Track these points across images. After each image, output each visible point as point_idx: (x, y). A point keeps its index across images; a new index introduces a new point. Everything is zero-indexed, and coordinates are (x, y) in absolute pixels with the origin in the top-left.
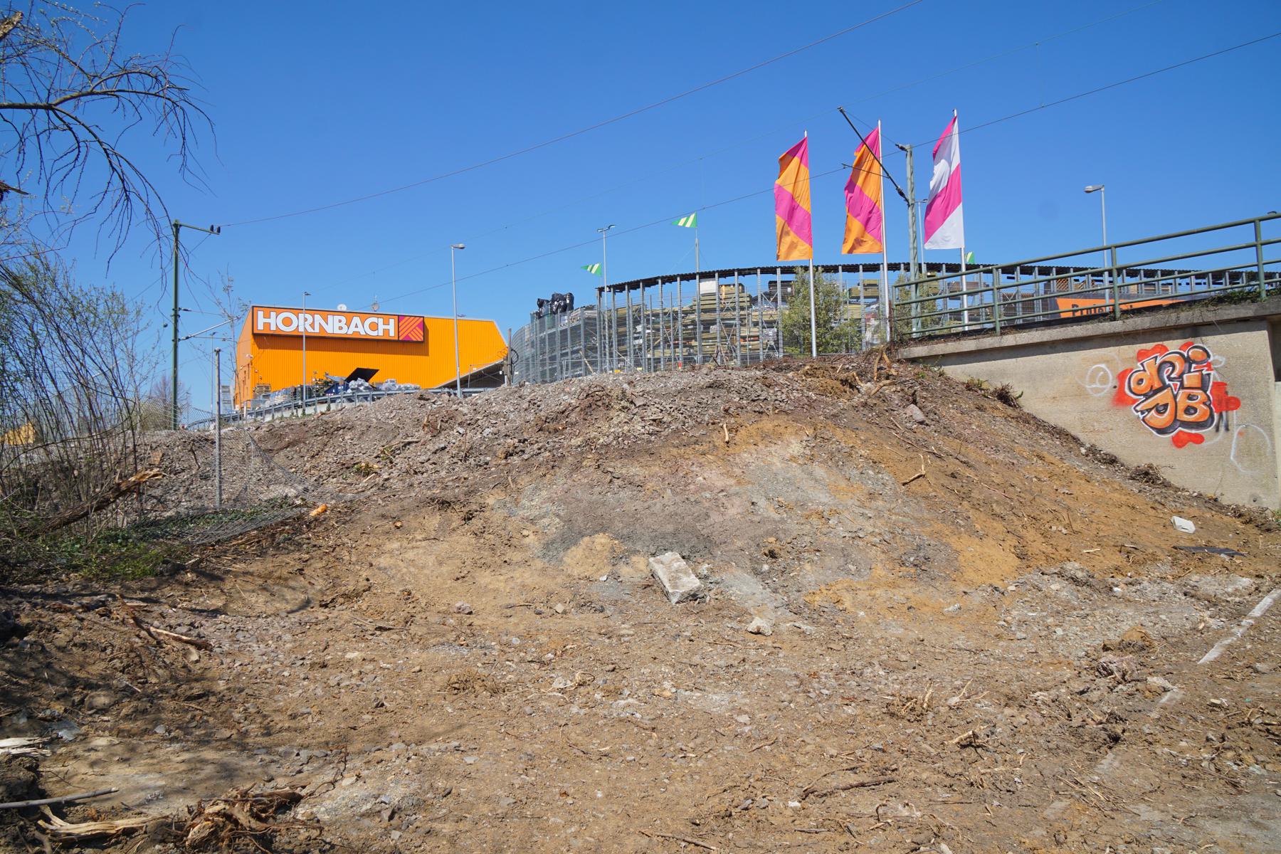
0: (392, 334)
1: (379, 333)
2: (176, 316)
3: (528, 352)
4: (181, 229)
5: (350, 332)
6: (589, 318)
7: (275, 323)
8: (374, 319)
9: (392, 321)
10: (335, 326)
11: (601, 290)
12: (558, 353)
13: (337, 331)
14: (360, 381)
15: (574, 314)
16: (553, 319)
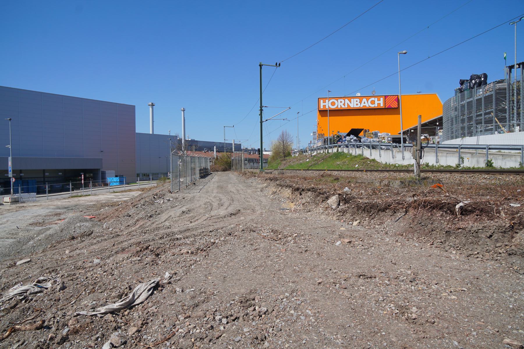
0: (382, 105)
1: (376, 105)
2: (261, 110)
3: (453, 114)
4: (263, 67)
5: (362, 106)
6: (500, 89)
7: (328, 105)
8: (373, 99)
9: (382, 99)
10: (354, 104)
11: (511, 67)
12: (474, 115)
13: (355, 106)
14: (352, 136)
15: (487, 87)
16: (471, 92)
